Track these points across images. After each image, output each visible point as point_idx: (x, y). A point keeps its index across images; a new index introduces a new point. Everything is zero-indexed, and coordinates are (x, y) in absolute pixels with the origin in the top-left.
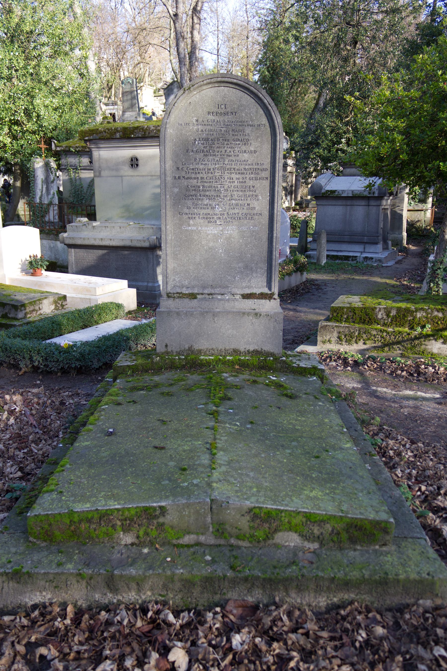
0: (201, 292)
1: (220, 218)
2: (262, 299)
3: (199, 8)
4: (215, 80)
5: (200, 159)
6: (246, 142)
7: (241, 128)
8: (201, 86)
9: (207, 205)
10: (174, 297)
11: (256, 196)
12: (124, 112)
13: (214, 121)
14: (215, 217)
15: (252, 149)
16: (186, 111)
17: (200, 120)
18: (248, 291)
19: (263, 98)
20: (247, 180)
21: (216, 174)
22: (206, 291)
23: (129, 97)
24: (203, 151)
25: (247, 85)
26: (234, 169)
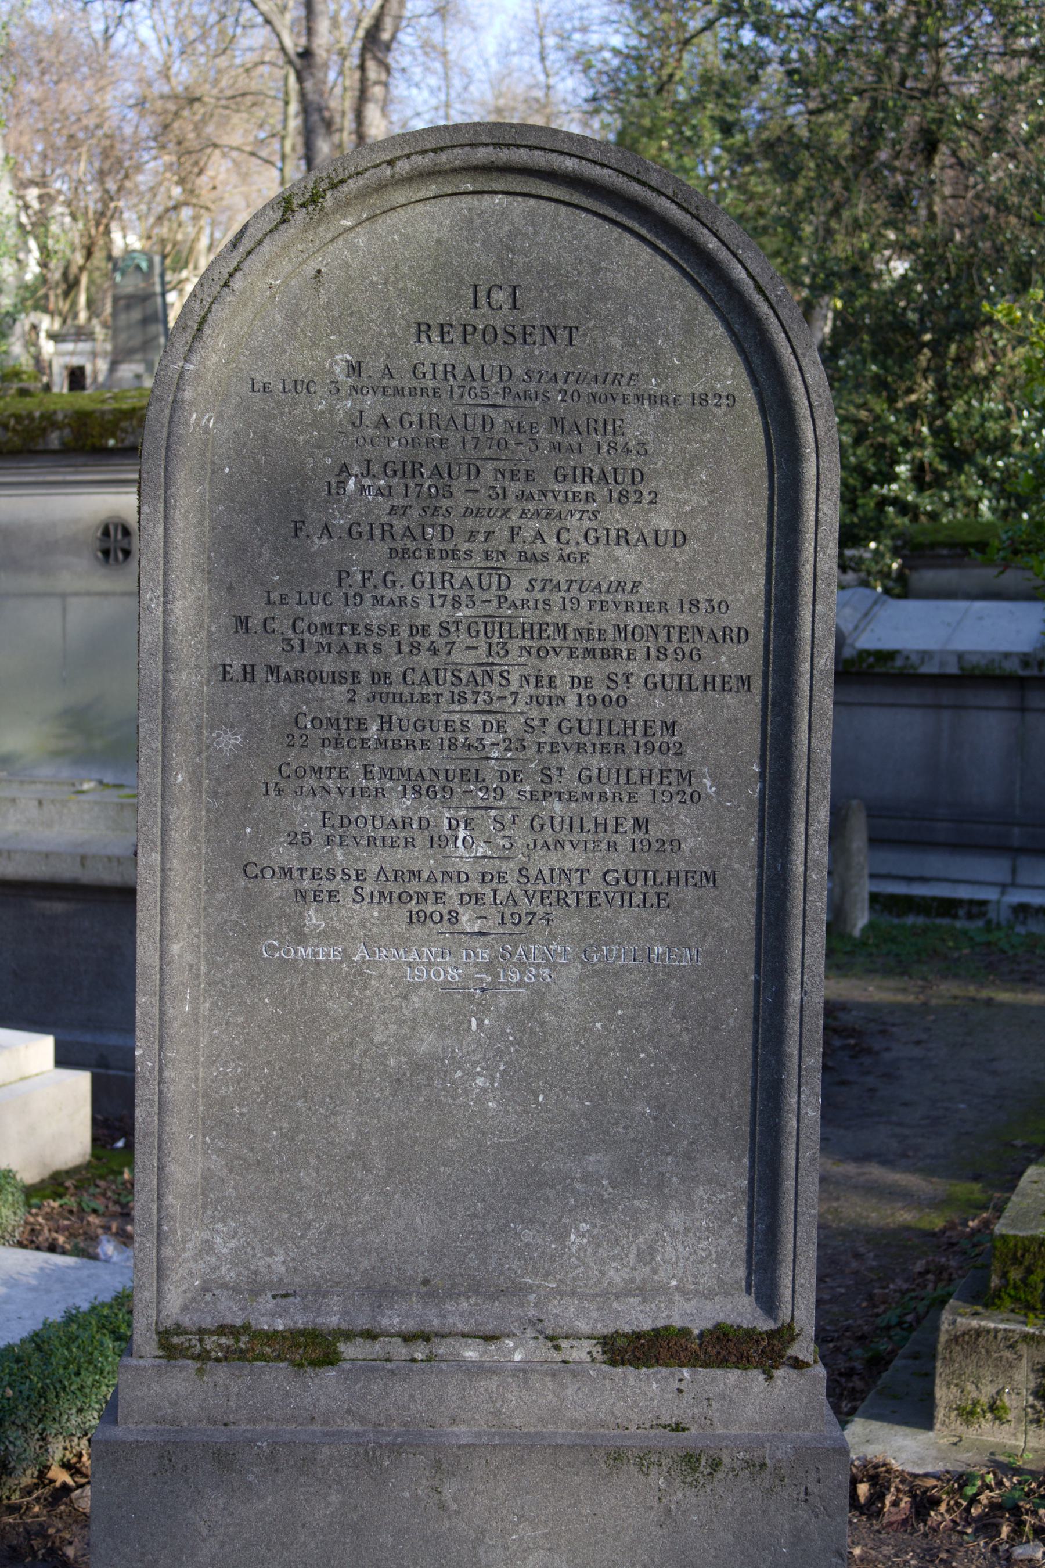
0: (362, 1322)
1: (477, 898)
2: (722, 1363)
3: (385, 36)
4: (459, 157)
5: (367, 574)
6: (629, 486)
7: (600, 412)
8: (381, 187)
9: (406, 823)
10: (203, 1357)
11: (686, 777)
12: (114, 365)
13: (449, 370)
14: (452, 891)
15: (665, 524)
16: (294, 316)
17: (374, 366)
18: (638, 1317)
19: (723, 255)
20: (636, 691)
21: (458, 656)
22: (392, 1320)
23: (136, 315)
24: (388, 532)
25: (635, 189)
26: (562, 629)
